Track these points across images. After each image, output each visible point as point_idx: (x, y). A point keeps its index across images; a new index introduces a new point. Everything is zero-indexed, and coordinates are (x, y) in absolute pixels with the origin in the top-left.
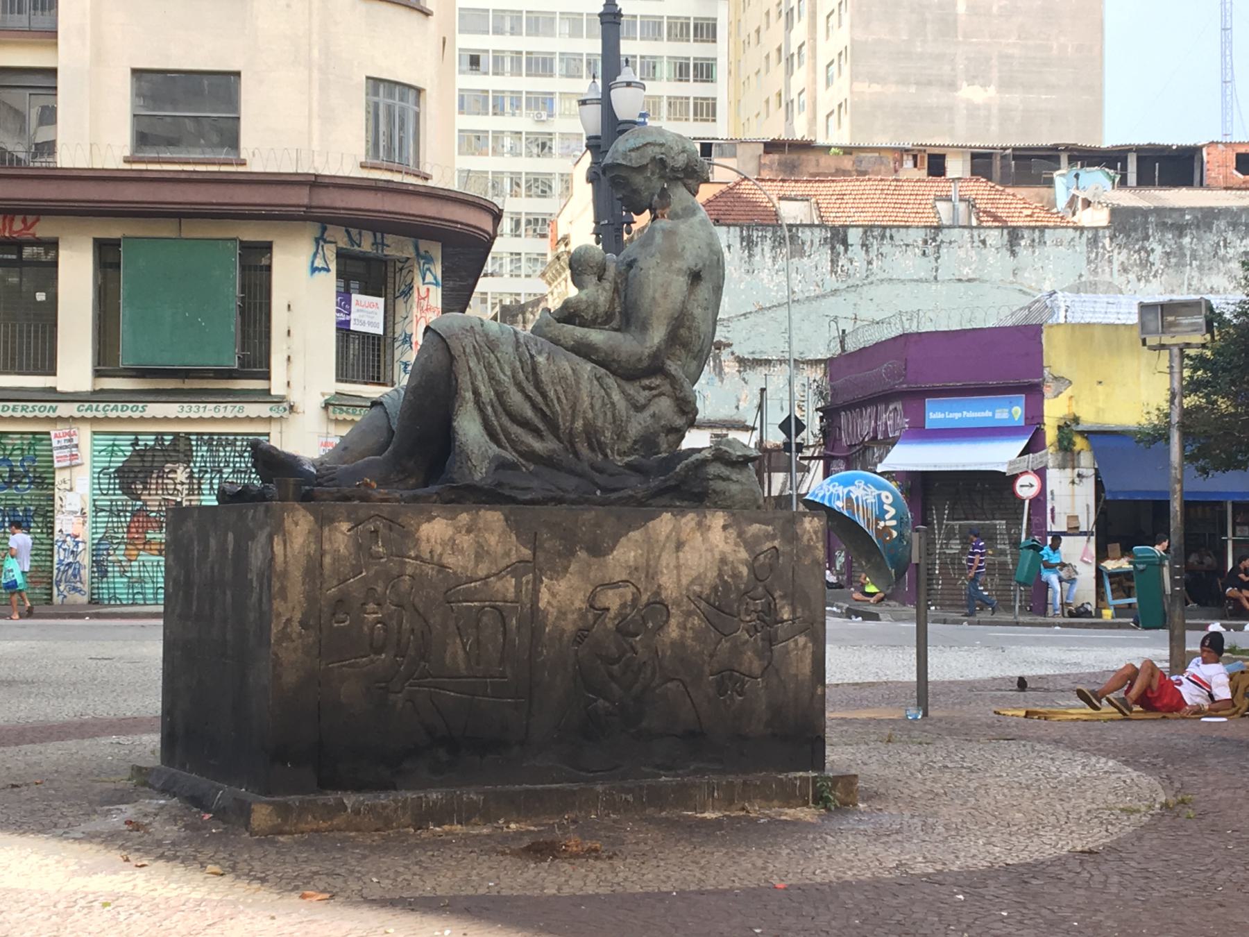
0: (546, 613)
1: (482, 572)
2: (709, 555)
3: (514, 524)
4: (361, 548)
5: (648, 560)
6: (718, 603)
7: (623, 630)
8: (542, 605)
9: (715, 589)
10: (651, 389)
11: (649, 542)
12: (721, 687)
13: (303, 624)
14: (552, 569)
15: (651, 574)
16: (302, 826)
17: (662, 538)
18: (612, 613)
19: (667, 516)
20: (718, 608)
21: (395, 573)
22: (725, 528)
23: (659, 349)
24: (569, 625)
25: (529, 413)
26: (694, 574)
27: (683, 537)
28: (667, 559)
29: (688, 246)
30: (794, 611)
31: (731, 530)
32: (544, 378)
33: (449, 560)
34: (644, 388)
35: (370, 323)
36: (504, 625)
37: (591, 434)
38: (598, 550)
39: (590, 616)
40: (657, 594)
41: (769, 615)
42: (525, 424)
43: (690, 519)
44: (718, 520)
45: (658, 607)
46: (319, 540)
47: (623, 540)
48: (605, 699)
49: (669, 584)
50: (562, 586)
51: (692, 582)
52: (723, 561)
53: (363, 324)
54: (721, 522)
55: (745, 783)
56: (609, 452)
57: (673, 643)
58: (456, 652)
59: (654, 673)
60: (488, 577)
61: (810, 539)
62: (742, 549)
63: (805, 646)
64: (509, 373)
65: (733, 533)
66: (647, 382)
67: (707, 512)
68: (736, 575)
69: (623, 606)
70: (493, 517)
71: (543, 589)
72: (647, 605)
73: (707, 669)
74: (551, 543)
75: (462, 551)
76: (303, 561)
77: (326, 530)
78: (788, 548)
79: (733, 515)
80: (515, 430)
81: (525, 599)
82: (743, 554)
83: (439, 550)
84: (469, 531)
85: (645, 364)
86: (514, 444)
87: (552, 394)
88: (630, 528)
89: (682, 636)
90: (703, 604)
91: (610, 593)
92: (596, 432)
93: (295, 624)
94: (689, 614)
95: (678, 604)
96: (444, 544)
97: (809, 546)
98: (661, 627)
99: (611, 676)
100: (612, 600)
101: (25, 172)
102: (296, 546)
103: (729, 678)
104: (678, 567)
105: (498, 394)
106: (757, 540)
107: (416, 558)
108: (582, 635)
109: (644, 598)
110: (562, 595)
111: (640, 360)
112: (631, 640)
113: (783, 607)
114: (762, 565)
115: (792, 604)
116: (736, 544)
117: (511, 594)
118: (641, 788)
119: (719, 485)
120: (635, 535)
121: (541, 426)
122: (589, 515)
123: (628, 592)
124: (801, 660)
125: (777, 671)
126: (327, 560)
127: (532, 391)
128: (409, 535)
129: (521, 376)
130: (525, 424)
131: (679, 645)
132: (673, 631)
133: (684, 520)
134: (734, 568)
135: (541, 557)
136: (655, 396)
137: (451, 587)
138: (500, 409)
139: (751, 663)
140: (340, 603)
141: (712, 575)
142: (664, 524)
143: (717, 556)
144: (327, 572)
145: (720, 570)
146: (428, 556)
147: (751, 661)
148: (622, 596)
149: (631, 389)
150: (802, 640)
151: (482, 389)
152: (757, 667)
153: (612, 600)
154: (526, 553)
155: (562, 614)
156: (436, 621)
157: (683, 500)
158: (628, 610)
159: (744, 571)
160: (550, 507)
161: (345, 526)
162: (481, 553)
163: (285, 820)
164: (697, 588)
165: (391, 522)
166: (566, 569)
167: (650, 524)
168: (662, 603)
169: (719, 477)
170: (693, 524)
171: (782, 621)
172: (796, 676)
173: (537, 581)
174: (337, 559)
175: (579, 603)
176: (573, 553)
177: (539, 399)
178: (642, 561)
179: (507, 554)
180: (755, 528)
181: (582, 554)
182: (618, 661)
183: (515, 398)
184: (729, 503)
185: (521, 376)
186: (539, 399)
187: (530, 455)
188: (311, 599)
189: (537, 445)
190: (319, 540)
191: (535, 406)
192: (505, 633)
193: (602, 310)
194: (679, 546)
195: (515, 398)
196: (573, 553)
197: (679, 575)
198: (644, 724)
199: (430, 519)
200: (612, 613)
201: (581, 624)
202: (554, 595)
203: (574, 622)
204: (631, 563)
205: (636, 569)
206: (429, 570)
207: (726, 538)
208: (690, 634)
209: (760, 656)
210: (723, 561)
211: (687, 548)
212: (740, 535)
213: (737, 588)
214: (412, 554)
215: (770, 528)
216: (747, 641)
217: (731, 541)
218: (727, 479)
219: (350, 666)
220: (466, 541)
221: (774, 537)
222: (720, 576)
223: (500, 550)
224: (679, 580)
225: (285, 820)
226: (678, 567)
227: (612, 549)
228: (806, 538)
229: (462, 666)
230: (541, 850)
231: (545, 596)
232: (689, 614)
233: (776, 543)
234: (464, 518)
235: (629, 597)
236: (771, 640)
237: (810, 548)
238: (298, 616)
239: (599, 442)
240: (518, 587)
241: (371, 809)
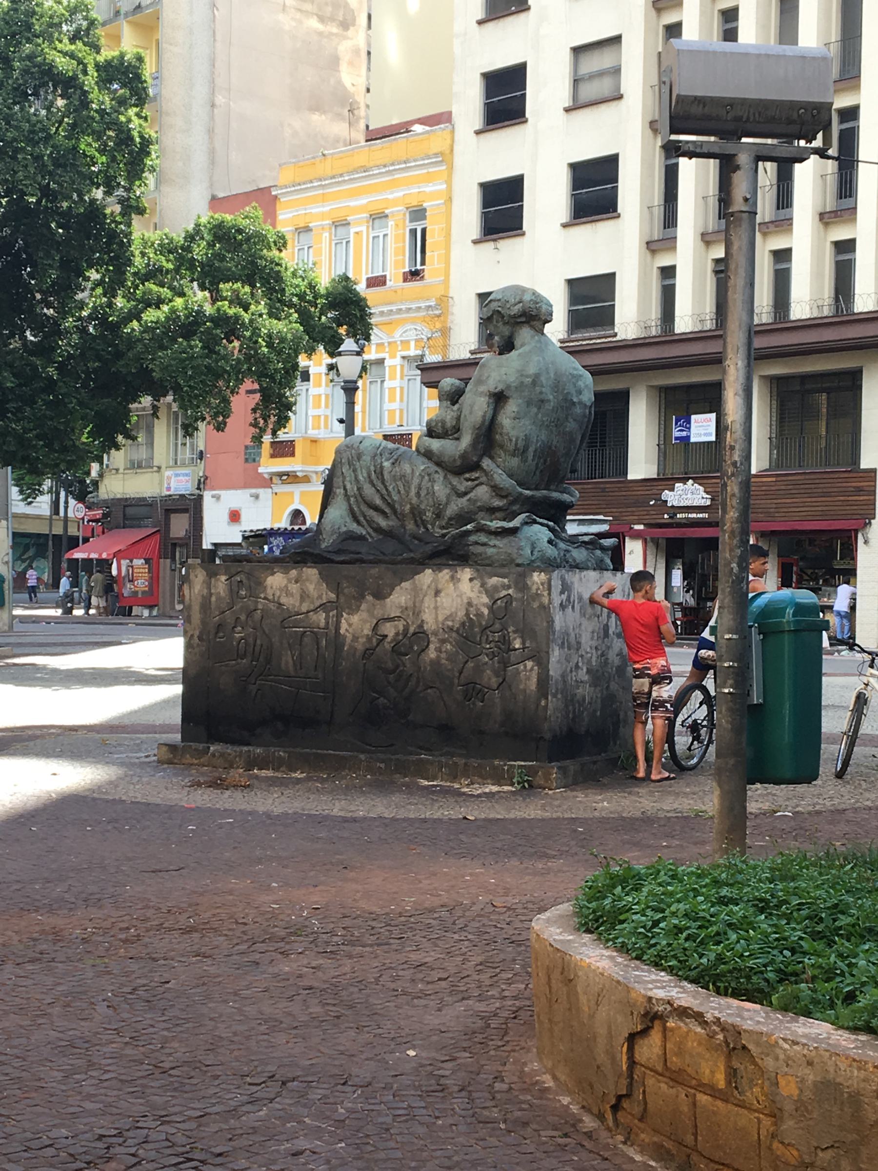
0: (345, 637)
1: (304, 609)
2: (459, 600)
3: (323, 577)
4: (233, 593)
5: (414, 603)
6: (468, 633)
7: (397, 650)
8: (342, 631)
9: (463, 624)
10: (473, 480)
11: (416, 590)
12: (467, 697)
13: (200, 638)
14: (350, 608)
15: (417, 613)
16: (184, 761)
17: (425, 587)
18: (389, 639)
19: (429, 571)
20: (466, 638)
21: (252, 608)
22: (471, 580)
23: (465, 451)
24: (360, 646)
25: (378, 502)
26: (448, 613)
27: (440, 586)
28: (428, 602)
29: (493, 374)
30: (523, 643)
31: (475, 582)
32: (386, 476)
33: (283, 600)
34: (468, 480)
35: (705, 434)
36: (318, 644)
37: (416, 513)
38: (380, 595)
39: (374, 640)
40: (421, 626)
41: (505, 644)
42: (376, 509)
43: (445, 574)
44: (466, 574)
45: (421, 635)
46: (209, 588)
47: (398, 588)
48: (385, 697)
49: (430, 620)
50: (355, 619)
51: (446, 619)
52: (470, 604)
53: (700, 435)
54: (469, 576)
55: (466, 764)
56: (430, 527)
57: (432, 661)
58: (287, 660)
59: (418, 682)
60: (308, 612)
61: (538, 589)
62: (484, 596)
63: (532, 669)
64: (365, 475)
65: (477, 583)
66: (467, 475)
67: (458, 569)
68: (479, 615)
69: (397, 634)
70: (311, 573)
71: (343, 621)
72: (414, 634)
73: (456, 681)
74: (349, 590)
75: (292, 595)
76: (200, 600)
77: (213, 580)
78: (520, 595)
79: (478, 570)
80: (371, 513)
81: (332, 628)
82: (485, 599)
83: (278, 593)
84: (296, 582)
85: (458, 463)
86: (370, 522)
87: (390, 488)
88: (403, 580)
89: (438, 657)
90: (454, 635)
91: (388, 625)
92: (420, 513)
93: (196, 637)
94: (443, 641)
95: (435, 633)
96: (281, 590)
97: (537, 594)
98: (423, 650)
99: (389, 683)
100: (389, 630)
101: (856, 317)
102: (196, 591)
103: (473, 690)
104: (436, 608)
105: (359, 489)
106: (496, 589)
107: (265, 598)
108: (368, 653)
109: (412, 629)
110: (356, 625)
111: (455, 460)
112: (403, 658)
113: (515, 639)
114: (500, 607)
115: (522, 637)
116: (480, 592)
117: (322, 623)
118: (391, 760)
119: (479, 549)
120: (406, 585)
121: (387, 510)
122: (375, 571)
123: (401, 625)
124: (528, 678)
125: (510, 687)
126: (213, 599)
127: (380, 486)
128: (260, 584)
129: (373, 476)
130: (376, 509)
131: (436, 663)
132: (432, 653)
133: (440, 575)
134: (478, 609)
135: (342, 599)
136: (477, 485)
137: (286, 618)
138: (360, 499)
139: (490, 679)
140: (220, 627)
141: (461, 614)
142: (427, 577)
143: (466, 601)
144: (213, 607)
145: (467, 610)
146: (271, 597)
147: (490, 678)
148: (396, 627)
149: (455, 481)
150: (529, 664)
151: (348, 486)
152: (494, 682)
153: (389, 630)
154: (333, 596)
155: (355, 638)
156: (275, 640)
157: (453, 560)
158: (400, 637)
159: (486, 611)
160: (356, 566)
161: (223, 578)
162: (304, 596)
163: (174, 757)
164: (450, 623)
165: (249, 575)
166: (358, 608)
167: (417, 577)
168: (424, 632)
169: (476, 543)
170: (447, 577)
171: (515, 650)
172: (525, 690)
173: (339, 616)
174: (219, 598)
175: (367, 631)
176: (363, 597)
177: (384, 492)
178: (410, 604)
179: (320, 597)
180: (495, 580)
181: (369, 598)
182: (394, 671)
183: (368, 491)
184: (487, 562)
185: (373, 476)
186: (384, 492)
187: (378, 530)
188: (204, 623)
189: (383, 523)
190: (209, 588)
191: (383, 498)
192: (318, 649)
193: (449, 425)
194: (437, 593)
195: (368, 491)
196: (363, 597)
197: (437, 615)
198: (410, 718)
199: (273, 574)
200: (389, 639)
201: (368, 646)
202: (350, 625)
203: (364, 643)
204: (403, 604)
205: (406, 608)
206: (272, 606)
207: (472, 587)
208: (443, 655)
209: (497, 674)
210: (470, 604)
211: (442, 594)
212: (482, 585)
213: (481, 624)
214: (262, 596)
215: (506, 581)
216: (486, 663)
217: (476, 589)
218: (484, 544)
219: (227, 665)
220: (294, 588)
221: (509, 587)
222: (467, 615)
223: (316, 595)
224: (437, 617)
225: (174, 757)
226: (436, 608)
227: (390, 594)
228: (535, 587)
229: (291, 668)
230: (218, 784)
231: (344, 626)
232: (443, 641)
233: (510, 591)
234: (294, 573)
235: (401, 628)
236: (505, 664)
237: (538, 595)
238: (197, 633)
239: (423, 521)
240: (327, 618)
241: (222, 755)
